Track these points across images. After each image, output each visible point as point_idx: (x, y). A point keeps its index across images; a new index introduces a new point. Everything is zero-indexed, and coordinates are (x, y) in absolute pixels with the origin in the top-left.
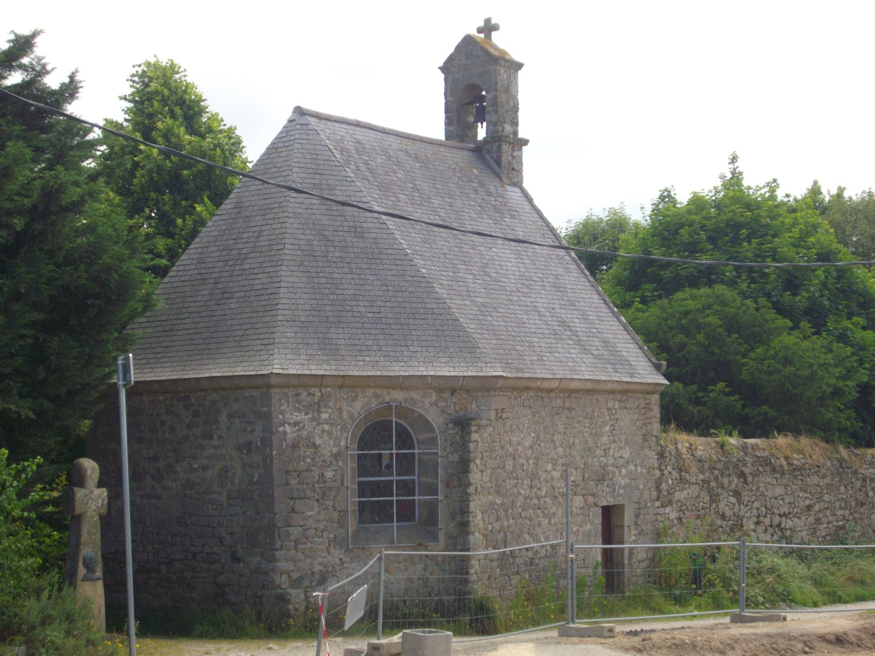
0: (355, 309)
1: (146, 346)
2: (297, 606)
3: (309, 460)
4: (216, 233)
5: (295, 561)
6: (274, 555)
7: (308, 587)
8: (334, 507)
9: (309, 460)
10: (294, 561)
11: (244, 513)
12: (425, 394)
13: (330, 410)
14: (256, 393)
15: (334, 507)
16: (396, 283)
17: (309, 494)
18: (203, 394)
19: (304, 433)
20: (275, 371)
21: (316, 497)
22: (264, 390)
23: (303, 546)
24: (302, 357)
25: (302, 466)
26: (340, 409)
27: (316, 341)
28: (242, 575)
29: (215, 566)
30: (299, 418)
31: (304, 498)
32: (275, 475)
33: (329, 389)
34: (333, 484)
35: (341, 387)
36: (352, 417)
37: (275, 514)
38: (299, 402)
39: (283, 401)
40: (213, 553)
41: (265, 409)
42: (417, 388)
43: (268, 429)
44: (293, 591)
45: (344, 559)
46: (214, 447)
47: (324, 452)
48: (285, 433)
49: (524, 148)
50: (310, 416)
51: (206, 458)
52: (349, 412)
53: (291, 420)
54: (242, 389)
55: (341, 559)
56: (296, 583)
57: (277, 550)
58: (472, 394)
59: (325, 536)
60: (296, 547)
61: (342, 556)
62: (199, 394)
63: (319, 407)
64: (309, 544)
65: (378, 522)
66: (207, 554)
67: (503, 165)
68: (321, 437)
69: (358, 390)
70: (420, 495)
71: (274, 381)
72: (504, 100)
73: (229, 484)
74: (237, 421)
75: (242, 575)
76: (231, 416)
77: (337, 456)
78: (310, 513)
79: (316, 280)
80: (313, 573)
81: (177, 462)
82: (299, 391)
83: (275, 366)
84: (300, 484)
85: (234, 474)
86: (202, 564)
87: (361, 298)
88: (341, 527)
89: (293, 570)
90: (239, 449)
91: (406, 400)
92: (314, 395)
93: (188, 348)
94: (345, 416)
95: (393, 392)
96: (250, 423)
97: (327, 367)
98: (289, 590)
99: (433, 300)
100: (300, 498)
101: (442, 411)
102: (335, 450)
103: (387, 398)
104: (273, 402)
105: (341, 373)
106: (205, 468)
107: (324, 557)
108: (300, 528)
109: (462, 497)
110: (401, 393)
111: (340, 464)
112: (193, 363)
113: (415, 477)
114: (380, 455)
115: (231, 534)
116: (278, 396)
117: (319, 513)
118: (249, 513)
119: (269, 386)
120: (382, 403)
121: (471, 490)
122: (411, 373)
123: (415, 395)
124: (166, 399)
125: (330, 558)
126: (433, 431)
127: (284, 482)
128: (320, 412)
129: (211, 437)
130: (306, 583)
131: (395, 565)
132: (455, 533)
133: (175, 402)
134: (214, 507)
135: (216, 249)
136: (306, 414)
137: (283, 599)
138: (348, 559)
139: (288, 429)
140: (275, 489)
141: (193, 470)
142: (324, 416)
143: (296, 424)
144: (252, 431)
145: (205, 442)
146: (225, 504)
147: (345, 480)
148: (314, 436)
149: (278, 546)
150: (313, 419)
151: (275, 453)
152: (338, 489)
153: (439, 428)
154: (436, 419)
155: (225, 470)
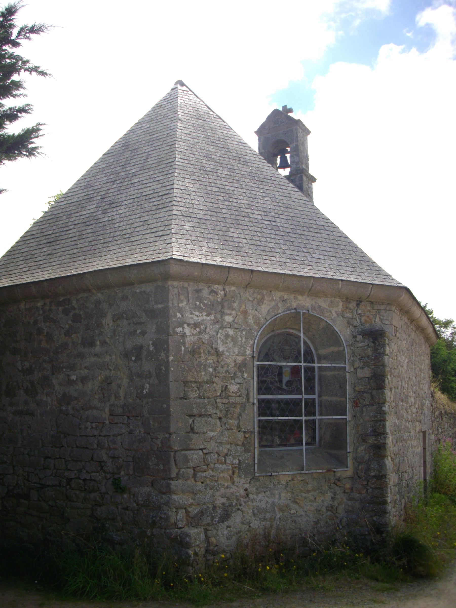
0: (251, 216)
1: (29, 257)
2: (197, 550)
3: (211, 370)
4: (104, 166)
5: (194, 493)
6: (168, 486)
7: (208, 525)
8: (239, 426)
9: (211, 370)
10: (193, 493)
11: (131, 432)
12: (332, 302)
13: (234, 312)
14: (149, 288)
15: (239, 426)
16: (285, 202)
17: (211, 410)
18: (85, 295)
19: (206, 337)
20: (174, 257)
21: (219, 415)
22: (159, 283)
23: (203, 474)
24: (204, 249)
25: (203, 376)
26: (245, 313)
27: (216, 237)
28: (127, 509)
29: (92, 495)
30: (200, 319)
31: (205, 415)
32: (171, 384)
33: (233, 288)
34: (238, 399)
35: (247, 286)
36: (257, 322)
37: (170, 434)
38: (200, 299)
39: (182, 298)
40: (91, 480)
41: (160, 306)
42: (326, 296)
43: (164, 330)
44: (193, 531)
45: (250, 489)
46: (96, 355)
47: (228, 361)
48: (184, 335)
49: (313, 183)
50: (212, 317)
51: (86, 368)
52: (255, 316)
53: (191, 321)
54: (131, 284)
55: (246, 490)
56: (194, 521)
57: (172, 479)
58: (376, 307)
59: (228, 461)
60: (195, 476)
61: (247, 486)
62: (81, 295)
63: (223, 307)
64: (210, 471)
65: (279, 446)
66: (85, 480)
67: (304, 189)
68: (225, 343)
69: (265, 292)
70: (321, 414)
71: (174, 269)
72: (302, 150)
73: (113, 397)
74: (125, 322)
75: (127, 509)
76: (117, 318)
77: (241, 367)
78: (211, 434)
79: (209, 188)
80: (214, 507)
81: (53, 374)
82: (200, 287)
83: (174, 253)
84: (200, 397)
85: (119, 386)
86: (78, 492)
87: (255, 208)
88: (247, 451)
89: (192, 504)
90: (126, 355)
91: (313, 308)
92: (216, 293)
93: (71, 252)
94: (251, 320)
95: (300, 297)
96: (140, 324)
97: (233, 261)
98: (186, 529)
99: (321, 219)
100: (200, 416)
101: (348, 323)
102: (240, 359)
103: (294, 305)
104: (171, 296)
105: (251, 268)
106: (84, 380)
107: (227, 487)
108: (200, 452)
109: (375, 416)
110: (308, 300)
111: (246, 375)
112: (76, 263)
113: (316, 397)
114: (281, 368)
115: (113, 457)
116: (176, 291)
117: (222, 434)
118: (137, 432)
119: (167, 277)
120: (288, 309)
121: (386, 408)
122: (322, 276)
123: (323, 303)
124: (45, 304)
125: (234, 489)
126: (341, 344)
127: (182, 395)
128: (223, 314)
129: (92, 344)
130: (207, 520)
131: (304, 495)
132: (367, 457)
133: (53, 307)
134: (94, 425)
135: (103, 176)
136: (208, 315)
137: (182, 543)
138: (254, 490)
139: (187, 331)
140: (172, 403)
141: (71, 383)
142: (228, 319)
143: (196, 325)
144: (143, 333)
145: (87, 350)
146: (107, 422)
147: (251, 394)
148: (216, 342)
149: (173, 475)
150: (216, 322)
151: (171, 358)
152: (243, 406)
153: (346, 341)
154: (344, 332)
155: (108, 382)
